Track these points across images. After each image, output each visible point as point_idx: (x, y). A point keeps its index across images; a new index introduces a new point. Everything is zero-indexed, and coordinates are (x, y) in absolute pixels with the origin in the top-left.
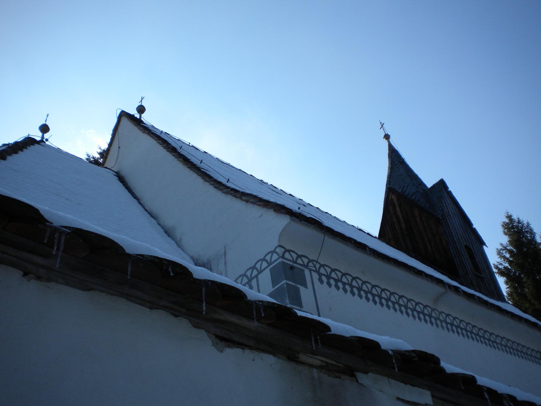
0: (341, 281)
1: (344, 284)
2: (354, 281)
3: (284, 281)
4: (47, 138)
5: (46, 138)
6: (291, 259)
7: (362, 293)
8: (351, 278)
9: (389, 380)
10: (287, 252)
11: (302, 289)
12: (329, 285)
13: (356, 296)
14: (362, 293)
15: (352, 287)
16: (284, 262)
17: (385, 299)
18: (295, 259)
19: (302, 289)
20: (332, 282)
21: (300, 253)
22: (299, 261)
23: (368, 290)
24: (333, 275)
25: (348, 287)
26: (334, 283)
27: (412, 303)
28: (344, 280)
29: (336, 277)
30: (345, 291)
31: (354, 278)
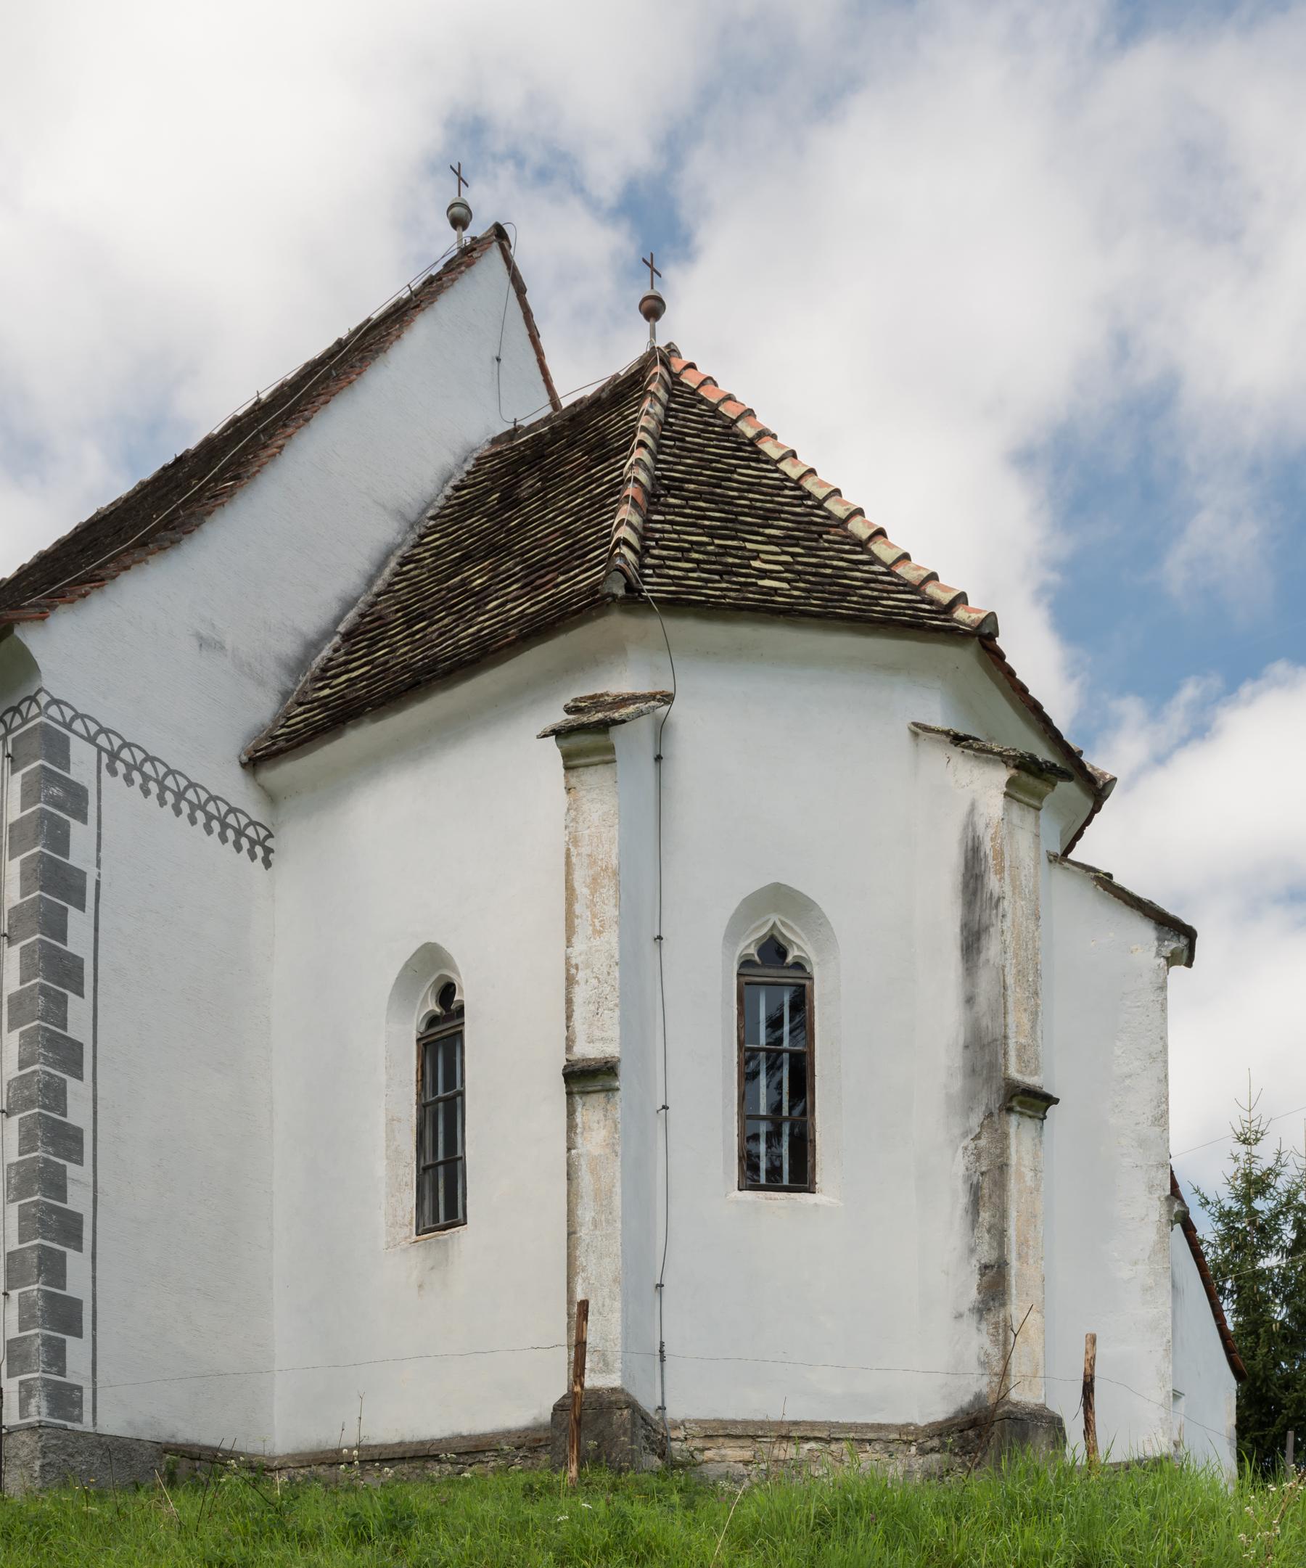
0: (202, 808)
1: (146, 778)
2: (252, 827)
3: (38, 893)
4: (501, 224)
5: (453, 234)
6: (60, 718)
7: (244, 842)
8: (165, 770)
9: (1037, 825)
10: (125, 747)
11: (73, 912)
12: (238, 848)
13: (230, 845)
14: (244, 842)
15: (225, 826)
16: (47, 725)
17: (172, 791)
18: (161, 775)
19: (73, 912)
20: (184, 806)
21: (214, 793)
22: (78, 725)
23: (133, 763)
24: (125, 754)
25: (153, 786)
26: (141, 782)
27: (135, 754)
28: (148, 768)
29: (254, 835)
30: (209, 830)
31: (232, 810)
